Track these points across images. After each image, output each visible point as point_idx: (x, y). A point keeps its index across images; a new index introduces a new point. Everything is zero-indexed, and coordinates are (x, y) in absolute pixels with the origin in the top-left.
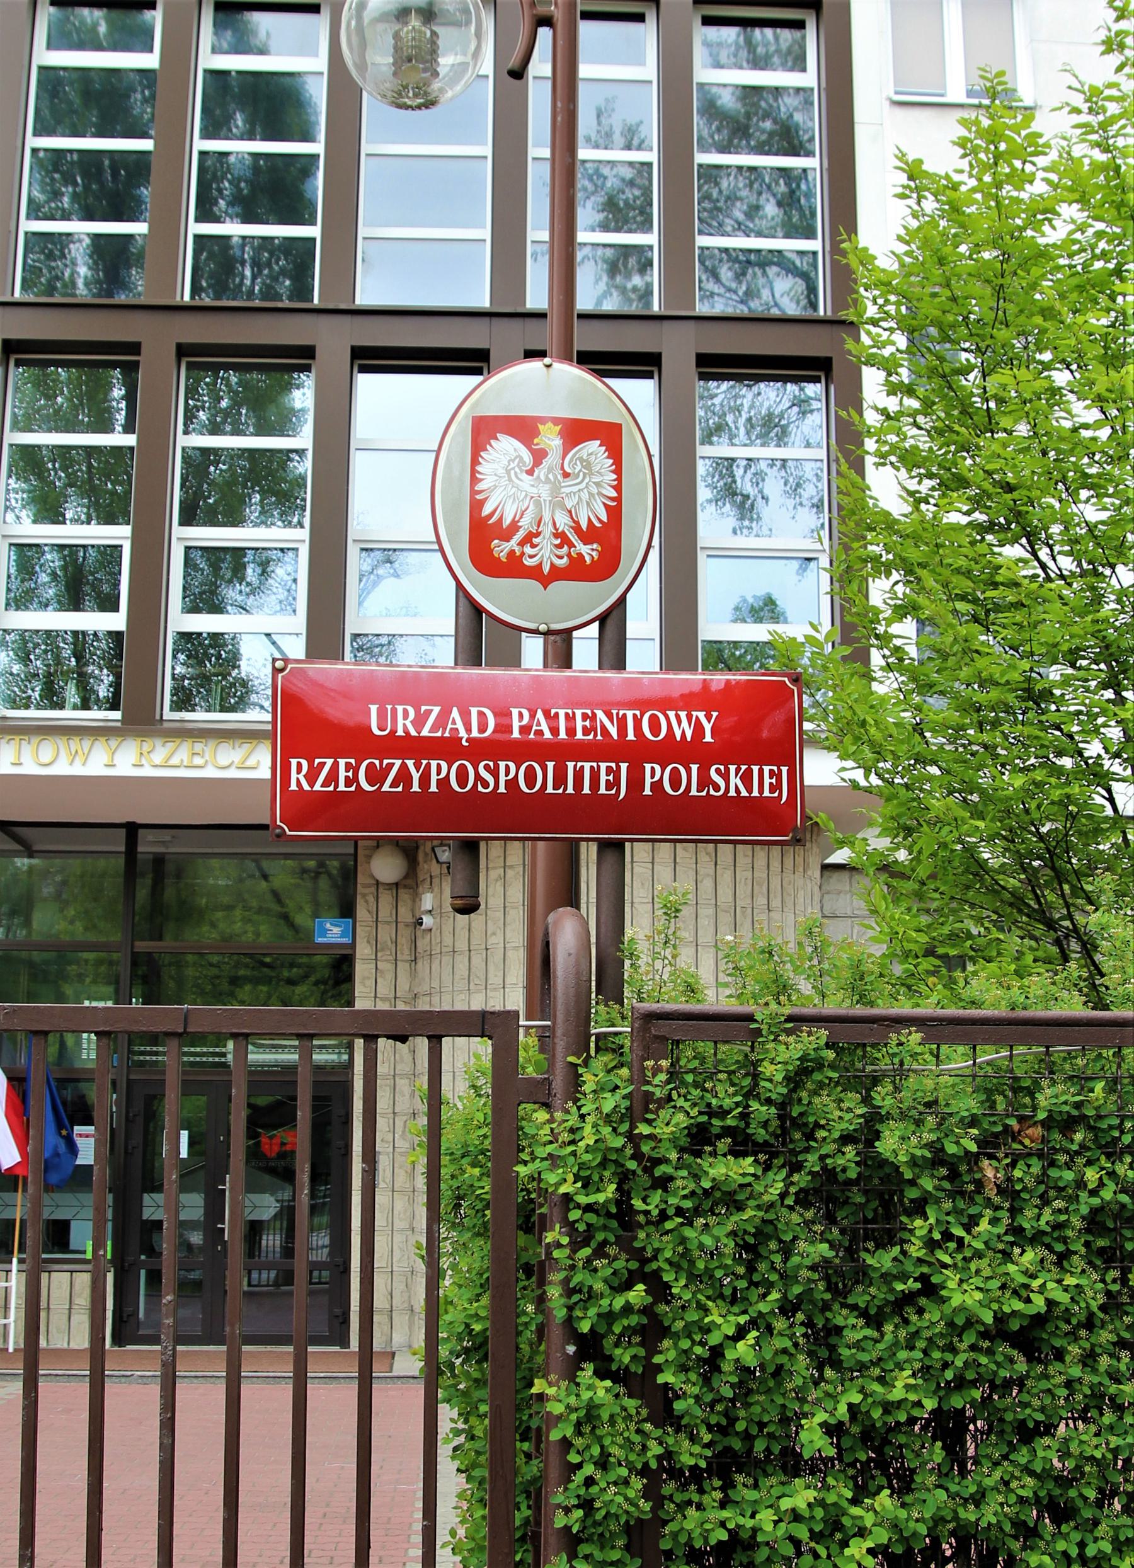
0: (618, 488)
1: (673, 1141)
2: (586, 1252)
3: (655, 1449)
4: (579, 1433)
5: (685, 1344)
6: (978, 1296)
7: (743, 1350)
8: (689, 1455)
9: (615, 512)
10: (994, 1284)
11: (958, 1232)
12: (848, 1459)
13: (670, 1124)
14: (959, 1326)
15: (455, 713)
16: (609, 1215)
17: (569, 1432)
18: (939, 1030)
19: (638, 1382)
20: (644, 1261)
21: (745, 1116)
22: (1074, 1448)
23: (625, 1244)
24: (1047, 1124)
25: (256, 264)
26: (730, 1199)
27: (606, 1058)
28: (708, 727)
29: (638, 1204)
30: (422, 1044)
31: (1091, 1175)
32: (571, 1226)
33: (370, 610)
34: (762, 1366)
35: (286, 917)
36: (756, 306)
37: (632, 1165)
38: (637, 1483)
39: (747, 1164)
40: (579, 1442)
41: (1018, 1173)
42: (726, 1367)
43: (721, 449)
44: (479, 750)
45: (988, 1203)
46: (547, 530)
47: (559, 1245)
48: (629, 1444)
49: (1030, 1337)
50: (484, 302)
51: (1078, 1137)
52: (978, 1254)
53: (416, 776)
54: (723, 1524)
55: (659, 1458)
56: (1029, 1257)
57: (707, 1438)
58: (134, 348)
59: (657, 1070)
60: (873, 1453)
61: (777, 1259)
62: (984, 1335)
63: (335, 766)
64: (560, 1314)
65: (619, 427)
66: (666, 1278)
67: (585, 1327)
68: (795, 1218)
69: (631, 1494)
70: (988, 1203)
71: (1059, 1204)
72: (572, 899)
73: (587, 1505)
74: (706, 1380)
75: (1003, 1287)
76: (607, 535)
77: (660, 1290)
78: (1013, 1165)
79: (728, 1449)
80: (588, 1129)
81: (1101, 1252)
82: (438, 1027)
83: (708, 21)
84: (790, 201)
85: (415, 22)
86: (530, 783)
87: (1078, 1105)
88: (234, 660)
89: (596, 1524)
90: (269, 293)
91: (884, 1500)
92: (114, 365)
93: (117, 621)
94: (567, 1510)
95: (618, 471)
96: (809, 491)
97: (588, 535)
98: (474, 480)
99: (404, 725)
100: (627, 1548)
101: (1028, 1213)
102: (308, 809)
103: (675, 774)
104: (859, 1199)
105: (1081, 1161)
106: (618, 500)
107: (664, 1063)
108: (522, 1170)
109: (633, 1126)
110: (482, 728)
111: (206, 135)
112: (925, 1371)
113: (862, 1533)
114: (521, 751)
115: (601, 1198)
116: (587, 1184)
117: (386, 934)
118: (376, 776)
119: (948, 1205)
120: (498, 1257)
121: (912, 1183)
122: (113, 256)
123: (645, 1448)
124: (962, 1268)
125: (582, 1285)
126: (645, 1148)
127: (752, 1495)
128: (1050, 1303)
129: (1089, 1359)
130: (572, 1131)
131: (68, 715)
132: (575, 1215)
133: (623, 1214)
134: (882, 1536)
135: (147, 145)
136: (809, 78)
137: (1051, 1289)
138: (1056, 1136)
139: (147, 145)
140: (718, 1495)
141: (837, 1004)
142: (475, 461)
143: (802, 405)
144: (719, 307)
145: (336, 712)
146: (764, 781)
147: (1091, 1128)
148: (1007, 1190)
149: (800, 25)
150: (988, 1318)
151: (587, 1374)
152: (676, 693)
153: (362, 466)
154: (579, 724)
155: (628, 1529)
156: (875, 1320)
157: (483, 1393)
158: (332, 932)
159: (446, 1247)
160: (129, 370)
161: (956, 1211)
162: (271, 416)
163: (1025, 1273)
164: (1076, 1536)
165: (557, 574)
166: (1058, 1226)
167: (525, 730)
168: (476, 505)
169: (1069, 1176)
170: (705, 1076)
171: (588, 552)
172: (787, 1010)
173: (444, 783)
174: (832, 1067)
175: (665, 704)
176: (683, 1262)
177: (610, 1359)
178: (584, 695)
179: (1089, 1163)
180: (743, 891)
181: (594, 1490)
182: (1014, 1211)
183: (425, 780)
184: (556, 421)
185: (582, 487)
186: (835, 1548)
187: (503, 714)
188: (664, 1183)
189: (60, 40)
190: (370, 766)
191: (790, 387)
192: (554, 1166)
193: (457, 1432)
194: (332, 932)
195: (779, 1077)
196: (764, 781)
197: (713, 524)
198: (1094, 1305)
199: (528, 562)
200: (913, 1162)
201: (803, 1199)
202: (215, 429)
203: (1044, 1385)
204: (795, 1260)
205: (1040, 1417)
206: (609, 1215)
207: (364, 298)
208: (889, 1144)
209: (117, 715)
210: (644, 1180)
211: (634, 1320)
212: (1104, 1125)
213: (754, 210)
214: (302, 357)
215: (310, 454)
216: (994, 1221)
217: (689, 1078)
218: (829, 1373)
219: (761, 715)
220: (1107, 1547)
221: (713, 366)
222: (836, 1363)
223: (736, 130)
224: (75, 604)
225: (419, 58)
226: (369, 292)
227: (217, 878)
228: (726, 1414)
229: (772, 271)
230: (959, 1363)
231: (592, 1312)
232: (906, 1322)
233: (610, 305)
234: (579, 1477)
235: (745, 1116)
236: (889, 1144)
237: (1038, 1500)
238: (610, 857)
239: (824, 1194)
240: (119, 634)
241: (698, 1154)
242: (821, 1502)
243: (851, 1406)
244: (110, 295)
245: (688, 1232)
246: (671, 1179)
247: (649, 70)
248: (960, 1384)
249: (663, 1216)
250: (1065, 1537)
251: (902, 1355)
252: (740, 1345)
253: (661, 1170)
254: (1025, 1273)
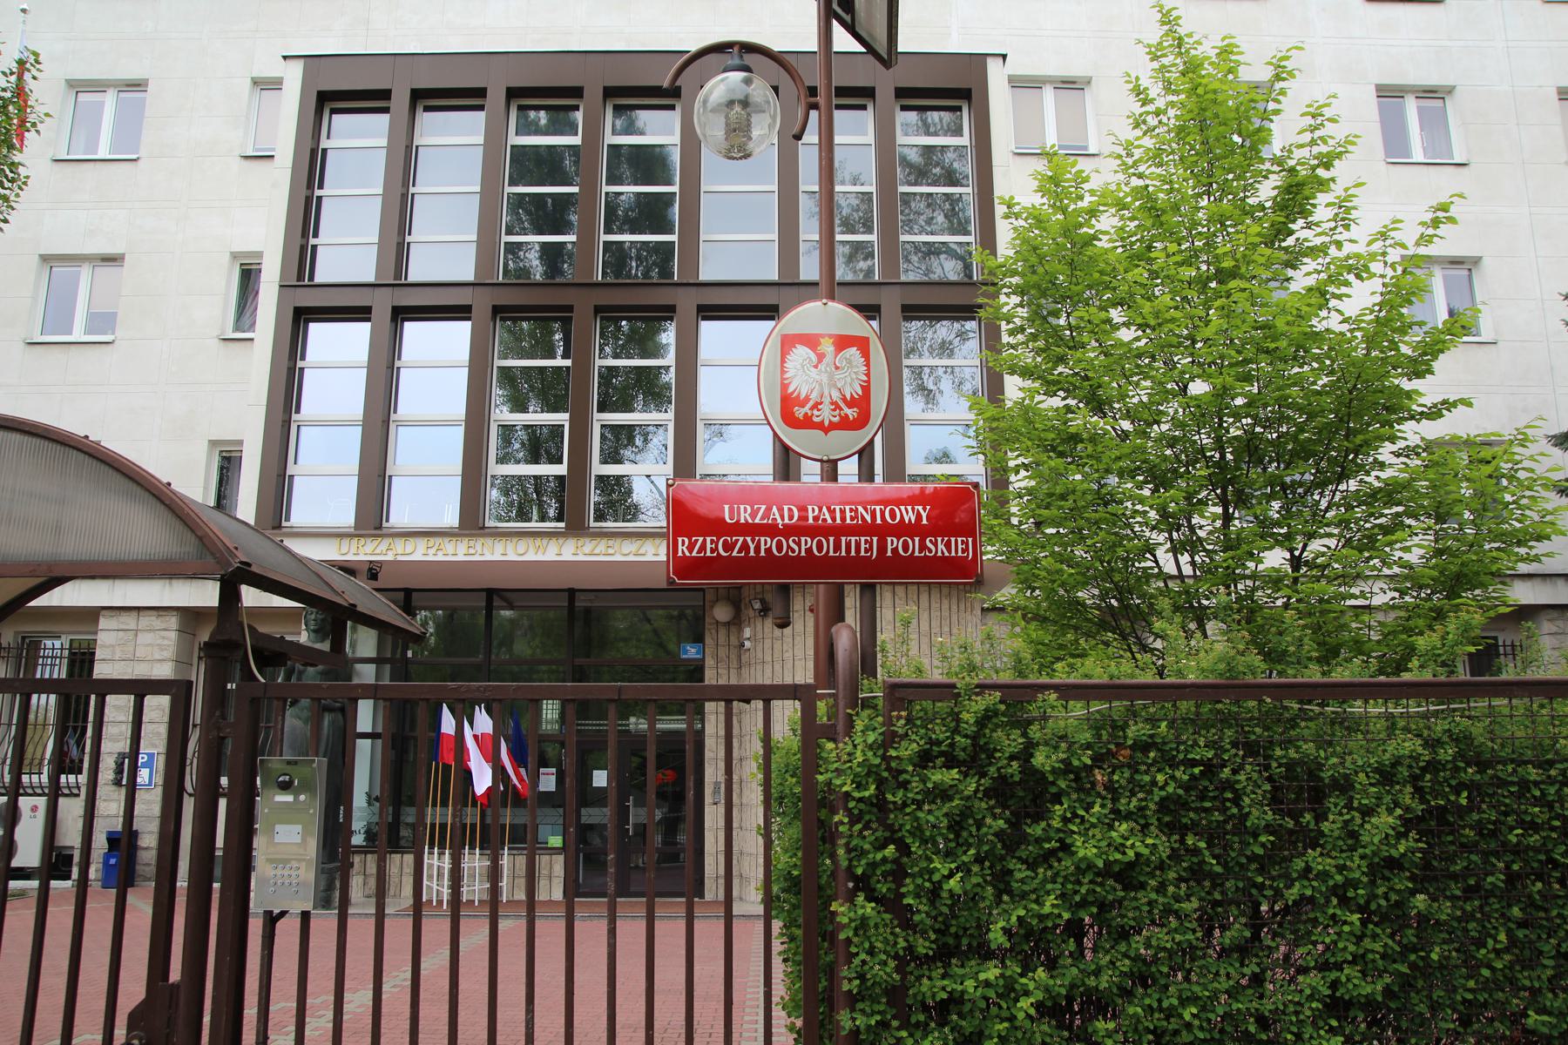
0: (868, 375)
1: (910, 760)
2: (859, 826)
3: (902, 944)
4: (856, 934)
5: (919, 881)
6: (1095, 851)
8: (923, 946)
9: (866, 389)
10: (1103, 844)
11: (1081, 812)
12: (1018, 949)
13: (907, 750)
14: (1085, 867)
15: (775, 509)
16: (872, 804)
17: (851, 934)
18: (1068, 692)
19: (891, 903)
20: (894, 832)
21: (952, 745)
22: (1154, 942)
23: (882, 822)
24: (1132, 747)
25: (639, 258)
26: (943, 793)
27: (867, 712)
28: (924, 515)
29: (889, 797)
30: (760, 704)
31: (1160, 778)
32: (849, 811)
33: (713, 458)
34: (965, 893)
36: (934, 277)
37: (885, 774)
38: (892, 964)
39: (954, 773)
40: (855, 940)
41: (1116, 778)
42: (945, 895)
43: (914, 361)
44: (789, 531)
45: (1099, 795)
46: (827, 401)
47: (842, 823)
48: (886, 941)
49: (1128, 875)
50: (774, 276)
51: (1152, 755)
52: (1094, 826)
53: (752, 547)
54: (944, 989)
55: (904, 949)
57: (933, 937)
58: (570, 308)
59: (899, 717)
60: (1033, 944)
61: (973, 829)
62: (1098, 874)
64: (845, 864)
67: (859, 871)
68: (984, 805)
69: (888, 970)
70: (1099, 795)
71: (1141, 795)
73: (862, 977)
74: (932, 903)
75: (1109, 845)
76: (862, 402)
77: (904, 849)
78: (1113, 773)
79: (945, 944)
80: (859, 753)
81: (1167, 824)
82: (769, 694)
83: (904, 108)
84: (951, 215)
85: (737, 108)
87: (1151, 736)
88: (629, 492)
89: (867, 989)
90: (646, 275)
91: (1041, 973)
92: (555, 319)
93: (561, 469)
94: (850, 980)
95: (868, 365)
96: (967, 387)
97: (851, 403)
98: (783, 372)
99: (744, 516)
100: (888, 1003)
101: (1123, 801)
102: (685, 567)
103: (905, 543)
104: (1021, 794)
105: (1154, 769)
106: (868, 382)
107: (903, 713)
108: (820, 778)
110: (791, 518)
112: (1062, 896)
113: (1027, 993)
114: (813, 531)
115: (867, 794)
117: (722, 652)
119: (1074, 796)
120: (806, 832)
121: (1053, 783)
122: (552, 254)
123: (896, 943)
124: (1084, 834)
126: (893, 764)
127: (960, 971)
128: (1137, 855)
129: (1161, 889)
130: (849, 754)
131: (534, 525)
132: (852, 804)
133: (880, 804)
134: (1039, 995)
135: (575, 189)
136: (964, 140)
137: (1137, 846)
138: (1139, 755)
139: (575, 189)
140: (941, 971)
141: (1006, 677)
142: (783, 361)
143: (962, 335)
144: (911, 277)
145: (703, 510)
146: (958, 547)
147: (1159, 750)
148: (1109, 786)
149: (959, 109)
150: (1100, 864)
153: (705, 377)
154: (848, 514)
155: (886, 992)
156: (1032, 865)
158: (691, 652)
159: (775, 827)
160: (566, 323)
161: (1080, 800)
162: (648, 347)
163: (1122, 837)
164: (1156, 996)
165: (833, 426)
166: (1141, 809)
167: (816, 518)
168: (784, 387)
169: (1147, 778)
170: (928, 720)
171: (851, 413)
172: (976, 681)
173: (768, 550)
174: (1003, 714)
175: (899, 502)
176: (917, 831)
177: (874, 890)
178: (849, 498)
179: (1159, 770)
180: (935, 623)
181: (866, 968)
182: (1115, 800)
183: (757, 549)
184: (830, 336)
185: (847, 375)
186: (1011, 1003)
187: (803, 509)
188: (904, 785)
189: (526, 128)
190: (725, 542)
191: (957, 325)
192: (839, 776)
193: (782, 934)
194: (691, 652)
195: (972, 721)
196: (958, 547)
198: (1164, 856)
199: (816, 420)
200: (1054, 771)
201: (988, 794)
202: (616, 356)
203: (1135, 904)
204: (985, 830)
205: (1133, 923)
206: (872, 804)
209: (562, 525)
210: (893, 783)
211: (888, 867)
212: (1167, 748)
213: (930, 221)
214: (668, 312)
215: (673, 370)
216: (1103, 806)
217: (919, 722)
218: (1006, 898)
219: (953, 509)
220: (1175, 1002)
221: (911, 312)
222: (1010, 893)
223: (920, 174)
224: (535, 460)
225: (740, 129)
227: (620, 623)
228: (944, 923)
229: (943, 256)
230: (1083, 891)
231: (863, 862)
232: (1051, 867)
233: (850, 277)
234: (857, 961)
235: (952, 745)
236: (1039, 759)
237: (1132, 973)
238: (868, 595)
239: (1000, 791)
241: (925, 768)
242: (1002, 975)
243: (1019, 917)
245: (920, 814)
246: (909, 782)
247: (870, 138)
248: (1084, 904)
249: (905, 805)
250: (1150, 996)
251: (1049, 886)
252: (952, 882)
253: (905, 776)
254: (1122, 837)
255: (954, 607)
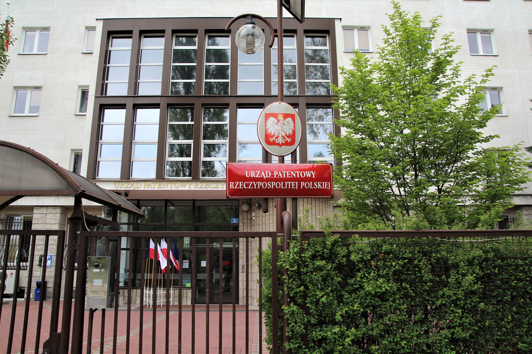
0: (294, 127)
1: (309, 257)
2: (291, 280)
3: (306, 320)
4: (290, 317)
5: (312, 298)
6: (371, 288)
7: (323, 299)
9: (294, 132)
10: (374, 286)
11: (367, 275)
13: (308, 254)
14: (368, 294)
15: (263, 172)
16: (296, 272)
17: (289, 316)
18: (362, 234)
19: (302, 306)
20: (303, 282)
21: (323, 252)
22: (392, 319)
23: (299, 278)
25: (217, 87)
26: (320, 269)
27: (294, 241)
28: (314, 175)
29: (302, 270)
30: (258, 239)
32: (288, 275)
33: (242, 155)
35: (224, 219)
36: (317, 94)
37: (300, 262)
38: (303, 326)
39: (324, 262)
40: (290, 318)
41: (379, 263)
42: (321, 303)
43: (310, 122)
44: (268, 180)
45: (373, 269)
46: (281, 136)
48: (301, 319)
49: (383, 296)
51: (391, 256)
52: (371, 280)
53: (255, 185)
54: (320, 335)
55: (307, 321)
56: (381, 280)
57: (317, 317)
58: (193, 104)
59: (305, 243)
60: (350, 320)
61: (330, 281)
63: (239, 183)
64: (287, 293)
65: (294, 115)
66: (308, 285)
67: (292, 295)
68: (334, 273)
69: (301, 329)
70: (373, 269)
71: (387, 269)
72: (285, 209)
73: (292, 331)
74: (316, 306)
75: (376, 286)
76: (292, 136)
77: (307, 288)
78: (378, 262)
79: (321, 320)
80: (291, 255)
81: (396, 279)
82: (261, 235)
84: (323, 73)
85: (250, 37)
86: (278, 186)
87: (391, 249)
88: (214, 167)
89: (294, 335)
90: (219, 93)
91: (353, 330)
92: (188, 108)
93: (190, 159)
94: (288, 332)
95: (294, 124)
96: (328, 131)
97: (289, 137)
98: (266, 126)
99: (253, 175)
100: (301, 340)
101: (381, 271)
102: (233, 192)
103: (307, 184)
104: (346, 269)
105: (391, 261)
106: (295, 129)
107: (307, 242)
108: (278, 263)
109: (301, 254)
110: (268, 175)
111: (207, 62)
112: (360, 304)
113: (348, 336)
114: (276, 180)
115: (294, 269)
116: (291, 267)
117: (245, 221)
118: (247, 185)
119: (365, 270)
120: (274, 282)
121: (357, 265)
122: (187, 86)
123: (304, 320)
125: (290, 286)
126: (303, 259)
127: (326, 329)
128: (386, 290)
129: (394, 301)
131: (181, 178)
132: (289, 272)
133: (299, 273)
134: (353, 337)
135: (195, 64)
136: (327, 47)
137: (386, 287)
138: (387, 256)
139: (195, 64)
140: (319, 329)
141: (342, 229)
142: (266, 122)
143: (326, 114)
144: (309, 94)
145: (239, 173)
146: (325, 185)
147: (393, 254)
148: (376, 266)
149: (325, 37)
150: (373, 293)
151: (292, 304)
152: (307, 168)
153: (239, 128)
154: (288, 174)
155: (301, 336)
156: (350, 293)
157: (271, 309)
158: (234, 221)
159: (263, 280)
160: (192, 109)
161: (366, 271)
162: (220, 118)
163: (381, 283)
164: (392, 337)
165: (283, 144)
166: (387, 274)
167: (277, 176)
168: (266, 131)
169: (389, 264)
170: (315, 244)
171: (289, 140)
172: (331, 231)
173: (261, 186)
174: (340, 242)
175: (305, 170)
176: (311, 282)
177: (297, 301)
178: (288, 169)
179: (393, 261)
180: (317, 211)
181: (294, 328)
182: (378, 271)
183: (257, 186)
184: (282, 114)
185: (287, 127)
186: (343, 340)
187: (272, 172)
188: (307, 266)
189: (178, 43)
190: (246, 184)
191: (325, 110)
192: (284, 263)
193: (265, 317)
194: (234, 221)
195: (330, 244)
196: (325, 185)
197: (310, 138)
199: (277, 142)
200: (358, 261)
202: (209, 121)
203: (385, 306)
204: (334, 281)
205: (384, 313)
206: (296, 272)
207: (239, 93)
208: (353, 257)
209: (191, 178)
211: (301, 294)
212: (396, 253)
213: (315, 75)
214: (227, 106)
215: (228, 125)
216: (374, 273)
218: (341, 304)
219: (324, 172)
220: (399, 339)
221: (309, 106)
222: (343, 302)
223: (312, 59)
224: (181, 156)
226: (240, 92)
227: (210, 211)
229: (320, 87)
230: (368, 302)
231: (293, 292)
232: (356, 294)
233: (288, 94)
234: (291, 326)
235: (323, 252)
237: (384, 329)
238: (294, 201)
239: (339, 268)
240: (191, 162)
241: (314, 260)
242: (340, 330)
243: (346, 311)
244: (188, 94)
245: (312, 276)
246: (308, 265)
247: (295, 47)
248: (368, 306)
249: (307, 273)
250: (390, 337)
251: (356, 300)
252: (323, 299)
253: (307, 263)
254: (381, 283)
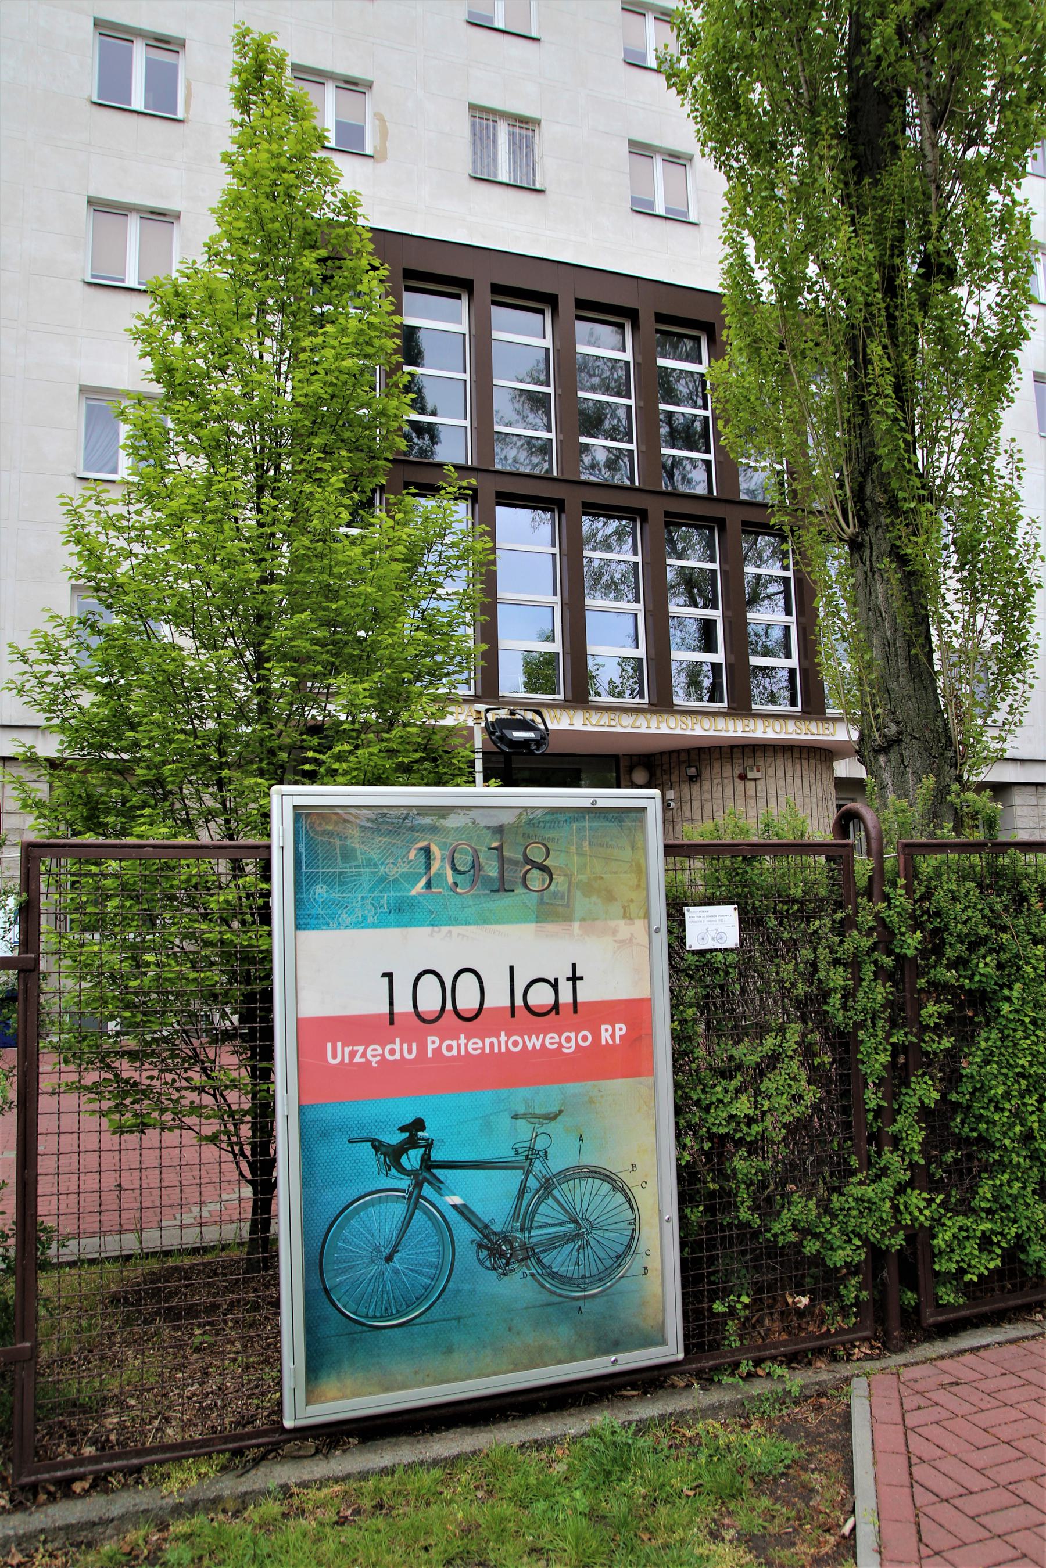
160: (722, 530)
247: (464, 328)
255: (789, 773)
